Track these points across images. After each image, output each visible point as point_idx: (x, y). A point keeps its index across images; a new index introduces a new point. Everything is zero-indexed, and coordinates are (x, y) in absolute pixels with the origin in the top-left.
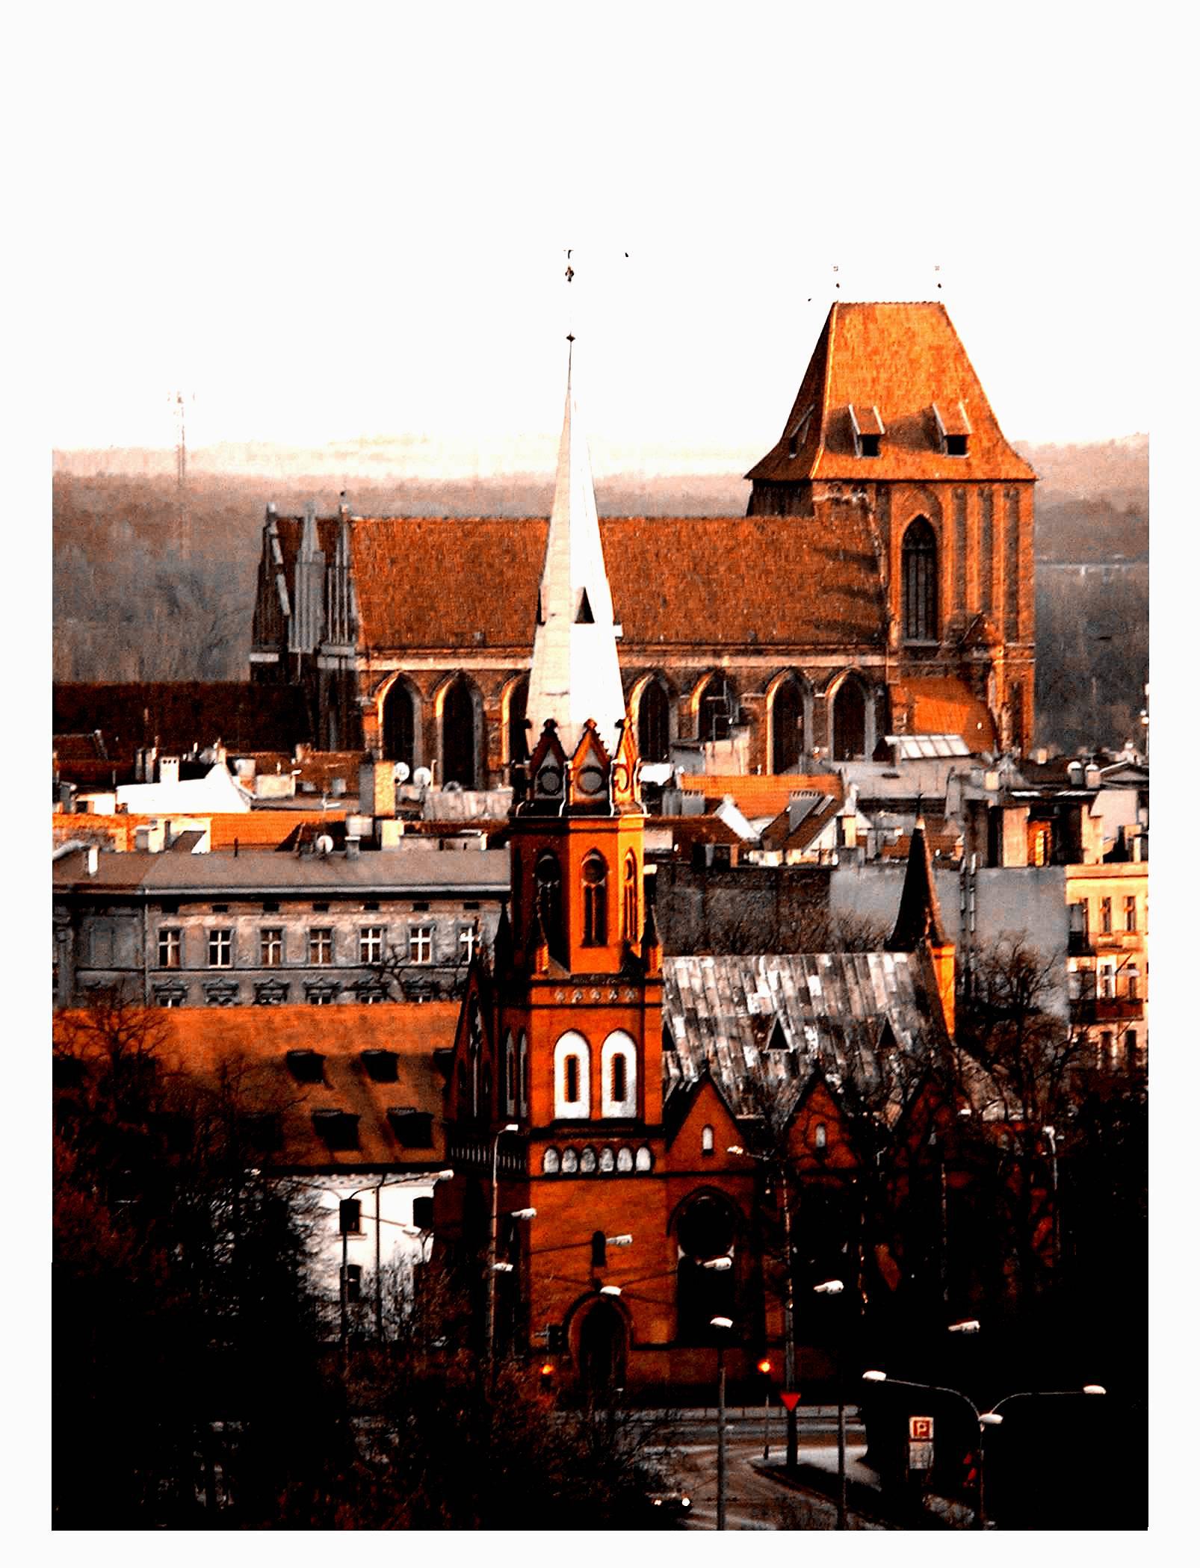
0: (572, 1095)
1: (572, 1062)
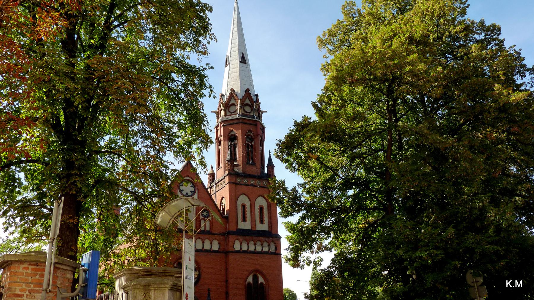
0: (244, 220)
1: (244, 206)
